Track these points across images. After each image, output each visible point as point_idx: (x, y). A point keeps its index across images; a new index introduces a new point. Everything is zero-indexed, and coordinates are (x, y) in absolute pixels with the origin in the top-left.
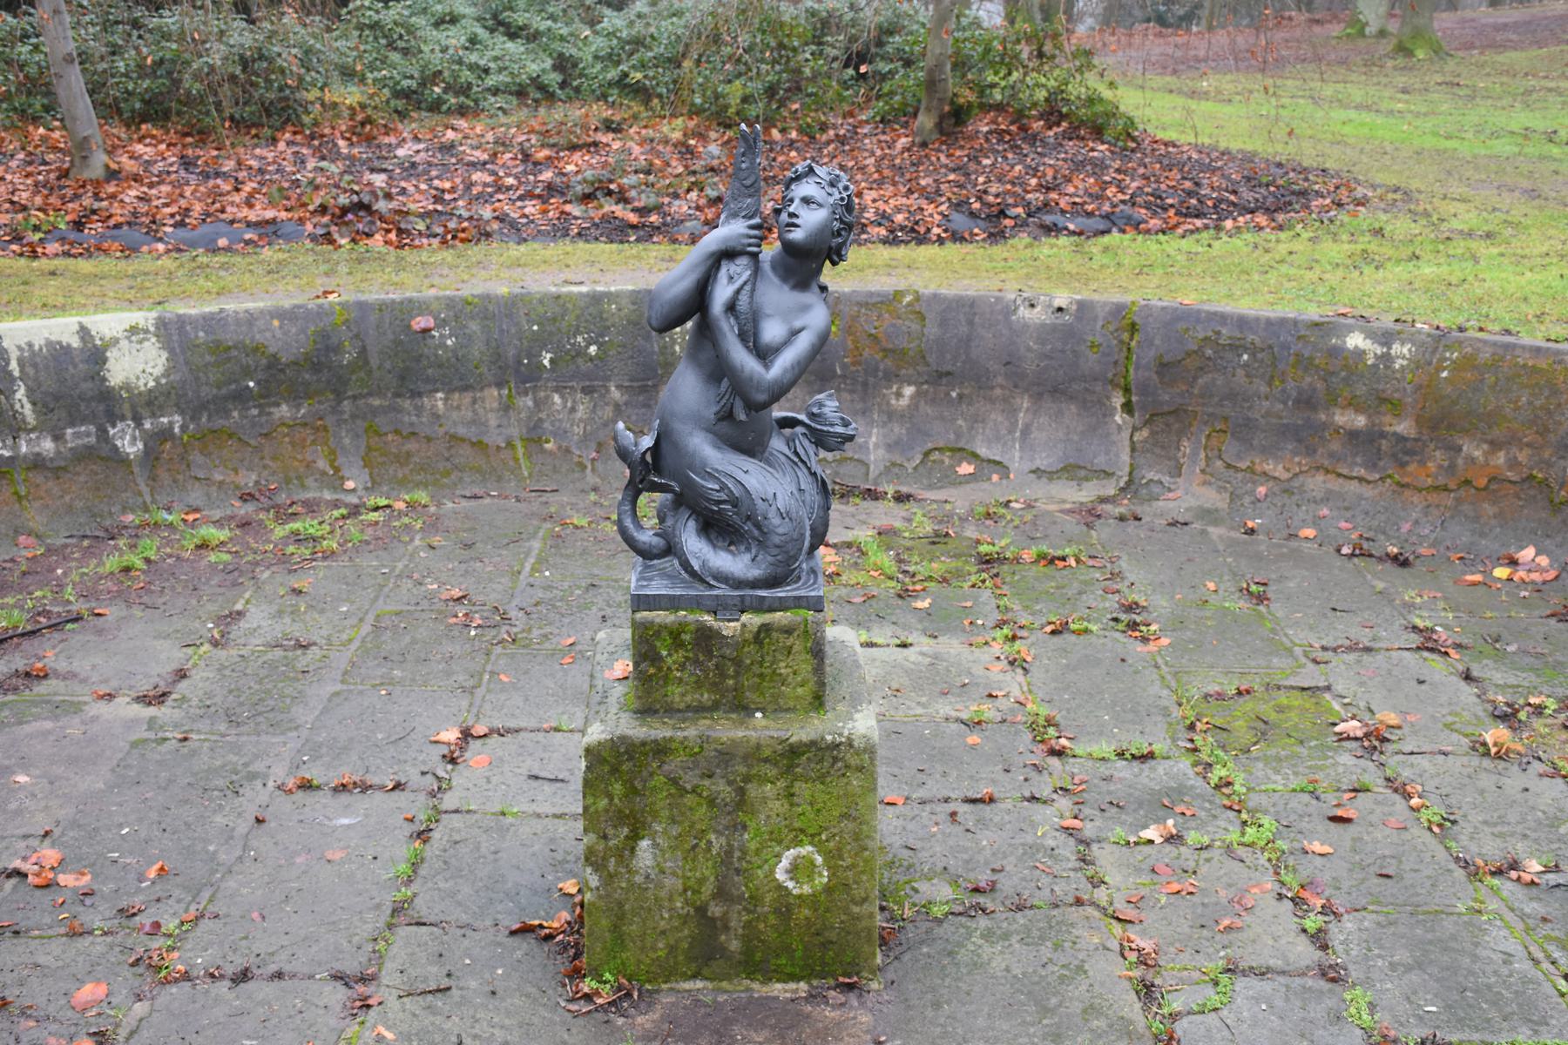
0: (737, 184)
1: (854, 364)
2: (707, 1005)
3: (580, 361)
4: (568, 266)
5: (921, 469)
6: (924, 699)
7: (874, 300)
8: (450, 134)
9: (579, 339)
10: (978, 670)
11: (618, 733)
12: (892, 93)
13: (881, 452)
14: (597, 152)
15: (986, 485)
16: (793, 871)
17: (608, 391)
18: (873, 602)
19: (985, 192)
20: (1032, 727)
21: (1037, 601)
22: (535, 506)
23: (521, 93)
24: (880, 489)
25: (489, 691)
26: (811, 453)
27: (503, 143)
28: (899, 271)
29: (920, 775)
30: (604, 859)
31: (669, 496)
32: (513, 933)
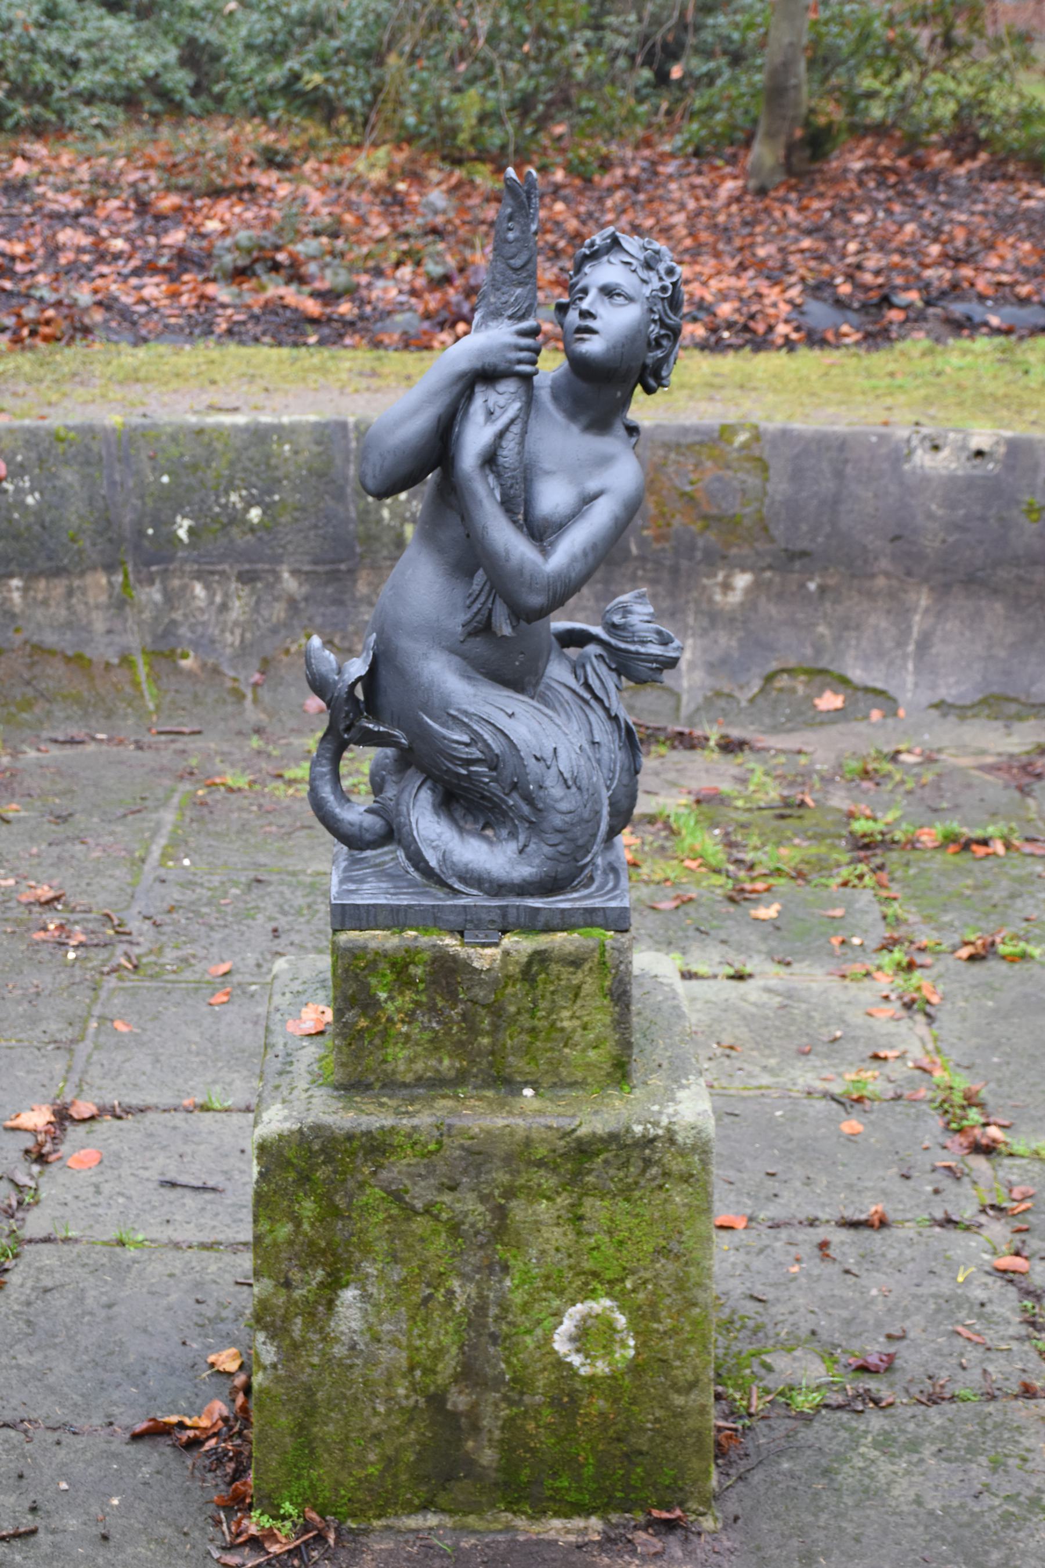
0: (501, 266)
1: (658, 538)
2: (444, 1555)
3: (235, 531)
4: (213, 382)
5: (761, 702)
6: (772, 1062)
7: (690, 439)
8: (20, 167)
9: (234, 497)
10: (855, 1017)
11: (310, 1120)
12: (710, 110)
13: (699, 676)
14: (254, 201)
15: (861, 727)
16: (581, 1338)
17: (278, 578)
18: (690, 908)
19: (859, 267)
20: (944, 1107)
21: (945, 908)
22: (166, 757)
23: (130, 101)
24: (698, 732)
25: (97, 1047)
26: (611, 687)
27: (105, 183)
28: (727, 393)
29: (769, 1183)
30: (285, 1319)
31: (390, 751)
32: (137, 1437)
